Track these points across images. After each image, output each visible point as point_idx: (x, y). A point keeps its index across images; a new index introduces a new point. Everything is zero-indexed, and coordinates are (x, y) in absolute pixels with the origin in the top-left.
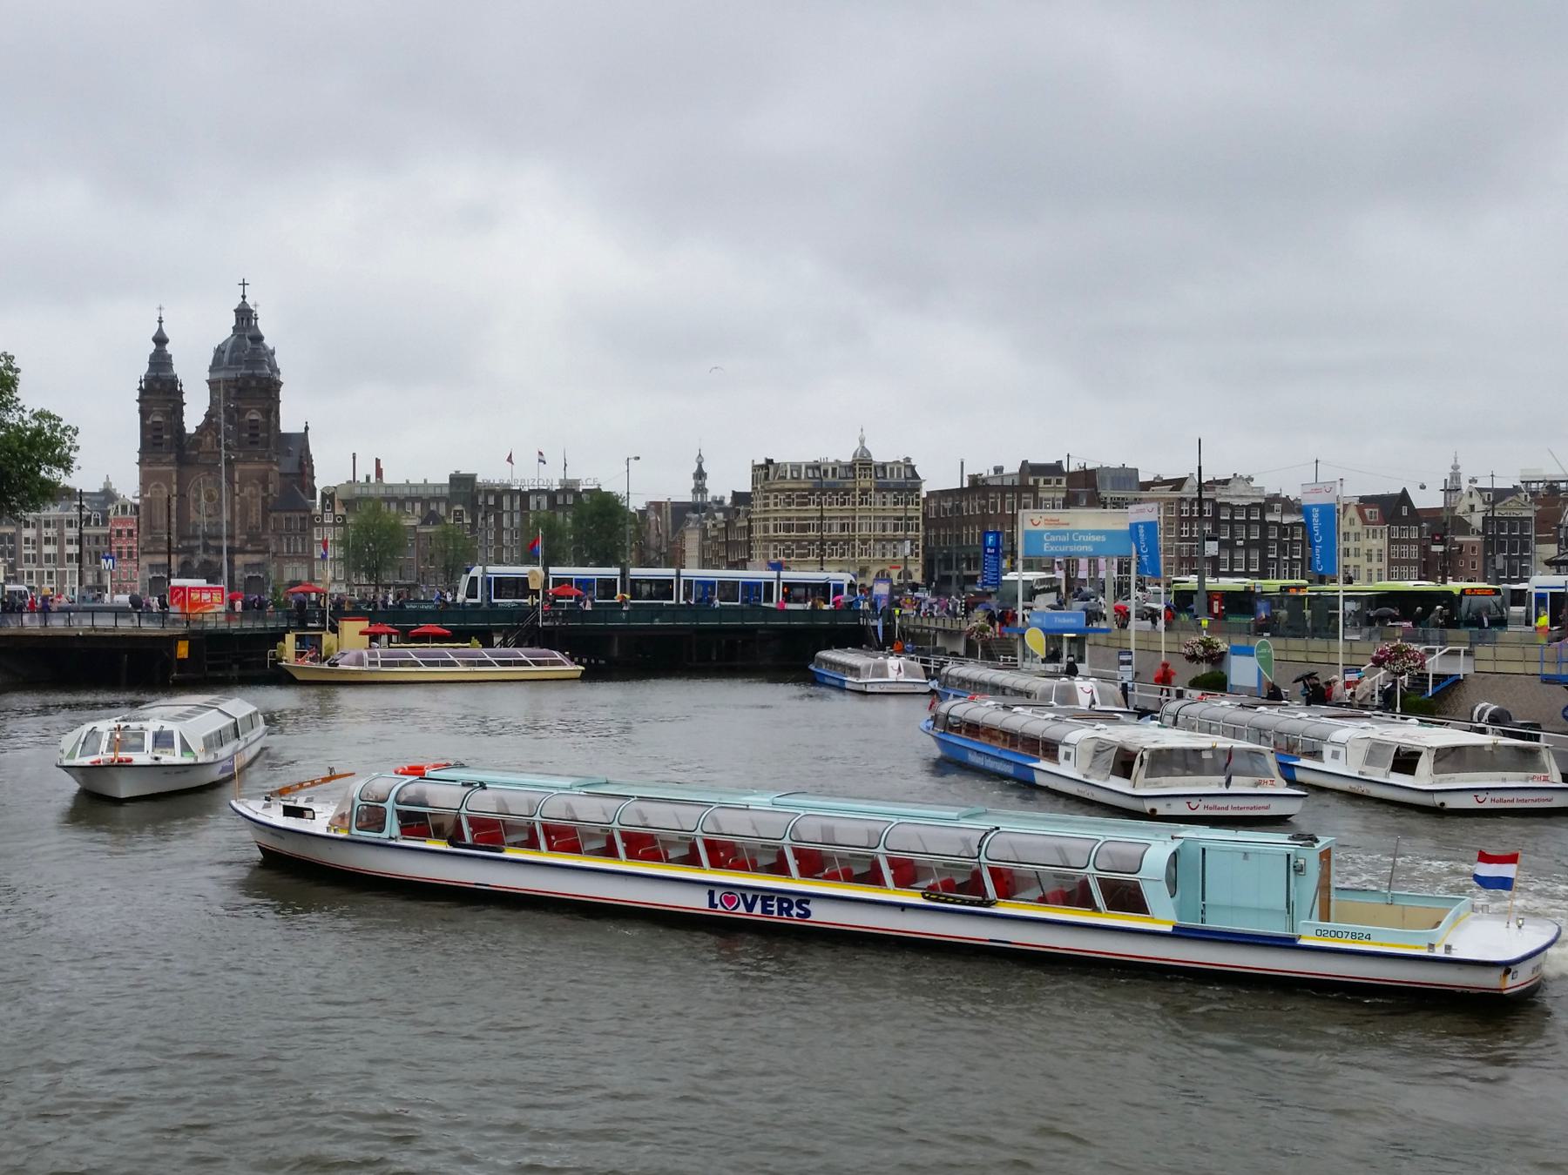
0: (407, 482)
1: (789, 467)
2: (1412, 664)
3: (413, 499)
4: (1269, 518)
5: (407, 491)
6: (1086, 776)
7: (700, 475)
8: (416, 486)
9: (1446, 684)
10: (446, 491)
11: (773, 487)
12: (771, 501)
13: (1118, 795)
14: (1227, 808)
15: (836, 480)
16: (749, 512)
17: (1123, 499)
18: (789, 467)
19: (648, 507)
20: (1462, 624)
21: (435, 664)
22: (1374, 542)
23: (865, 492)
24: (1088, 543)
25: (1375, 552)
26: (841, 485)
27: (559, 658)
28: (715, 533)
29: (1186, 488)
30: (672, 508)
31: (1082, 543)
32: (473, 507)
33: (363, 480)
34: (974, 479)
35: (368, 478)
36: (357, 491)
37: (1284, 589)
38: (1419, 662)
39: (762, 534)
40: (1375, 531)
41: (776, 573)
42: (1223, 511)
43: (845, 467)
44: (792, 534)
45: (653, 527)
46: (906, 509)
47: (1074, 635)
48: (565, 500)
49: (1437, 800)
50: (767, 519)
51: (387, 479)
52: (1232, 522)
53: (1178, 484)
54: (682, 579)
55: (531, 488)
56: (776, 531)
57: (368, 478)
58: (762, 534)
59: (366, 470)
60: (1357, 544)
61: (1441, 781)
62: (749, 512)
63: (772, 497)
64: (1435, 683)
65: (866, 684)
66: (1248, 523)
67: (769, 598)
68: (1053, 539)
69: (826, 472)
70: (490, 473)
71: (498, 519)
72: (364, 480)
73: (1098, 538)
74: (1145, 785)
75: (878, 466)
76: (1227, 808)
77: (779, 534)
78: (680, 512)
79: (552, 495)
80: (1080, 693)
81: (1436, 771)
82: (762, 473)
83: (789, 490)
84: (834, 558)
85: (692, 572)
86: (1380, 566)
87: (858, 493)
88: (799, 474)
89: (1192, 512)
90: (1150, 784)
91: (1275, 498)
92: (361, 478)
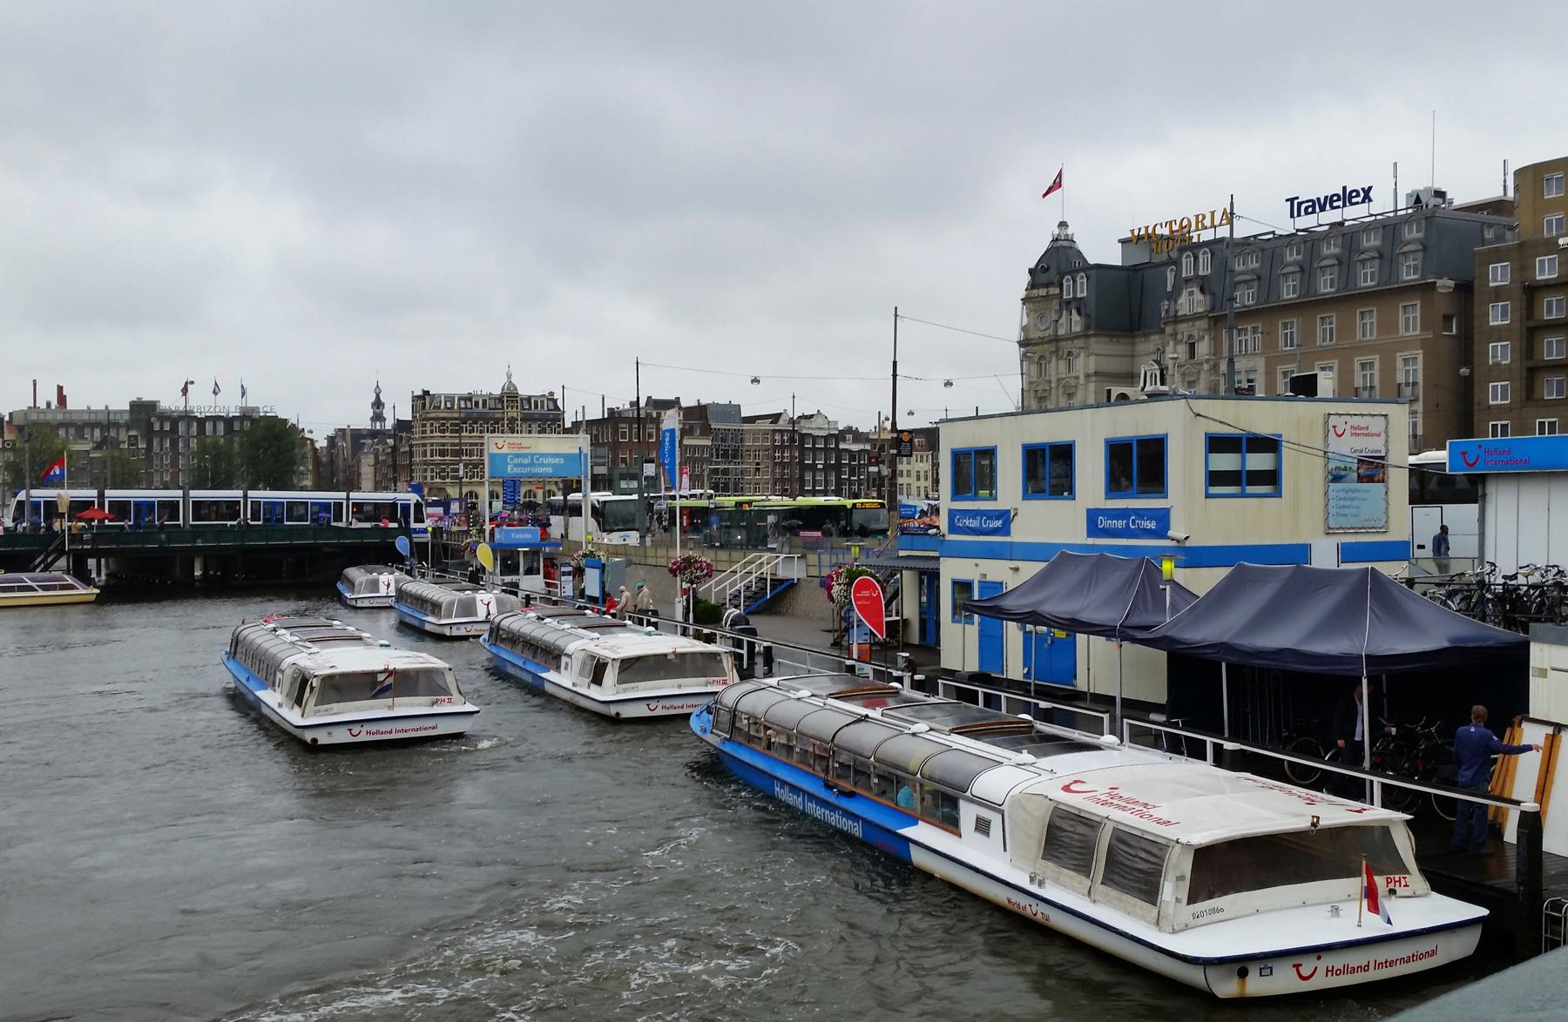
0: (107, 407)
1: (443, 397)
2: (699, 573)
3: (93, 425)
4: (842, 446)
5: (86, 417)
6: (574, 685)
7: (378, 404)
8: (96, 412)
9: (782, 587)
10: (127, 417)
11: (429, 416)
12: (428, 429)
13: (595, 702)
14: (391, 732)
15: (485, 410)
16: (410, 438)
17: (729, 430)
18: (443, 397)
19: (336, 434)
20: (853, 533)
21: (54, 588)
22: (922, 465)
23: (512, 420)
24: (548, 465)
25: (922, 474)
26: (491, 415)
27: (71, 582)
28: (384, 458)
29: (781, 422)
30: (351, 435)
31: (542, 465)
32: (149, 433)
33: (44, 406)
34: (611, 411)
35: (49, 405)
36: (34, 417)
37: (739, 504)
38: (705, 571)
39: (421, 458)
40: (922, 457)
41: (345, 493)
42: (818, 440)
43: (495, 399)
44: (447, 458)
45: (341, 452)
46: (460, 437)
47: (527, 549)
48: (162, 427)
49: (613, 710)
50: (424, 445)
51: (70, 406)
52: (814, 449)
53: (775, 418)
54: (249, 500)
55: (208, 414)
56: (432, 456)
57: (49, 405)
58: (421, 458)
59: (48, 396)
60: (909, 467)
61: (625, 691)
62: (410, 438)
63: (428, 425)
64: (773, 587)
65: (356, 599)
66: (826, 449)
67: (338, 518)
68: (516, 461)
69: (477, 403)
70: (170, 401)
71: (174, 444)
72: (45, 407)
73: (556, 461)
74: (316, 712)
75: (525, 399)
76: (391, 732)
77: (435, 458)
78: (357, 436)
79: (229, 421)
80: (479, 605)
81: (620, 682)
82: (420, 402)
83: (444, 419)
84: (475, 479)
85: (366, 495)
86: (926, 484)
87: (506, 422)
88: (453, 405)
89: (783, 441)
90: (319, 711)
91: (849, 430)
92: (42, 405)
